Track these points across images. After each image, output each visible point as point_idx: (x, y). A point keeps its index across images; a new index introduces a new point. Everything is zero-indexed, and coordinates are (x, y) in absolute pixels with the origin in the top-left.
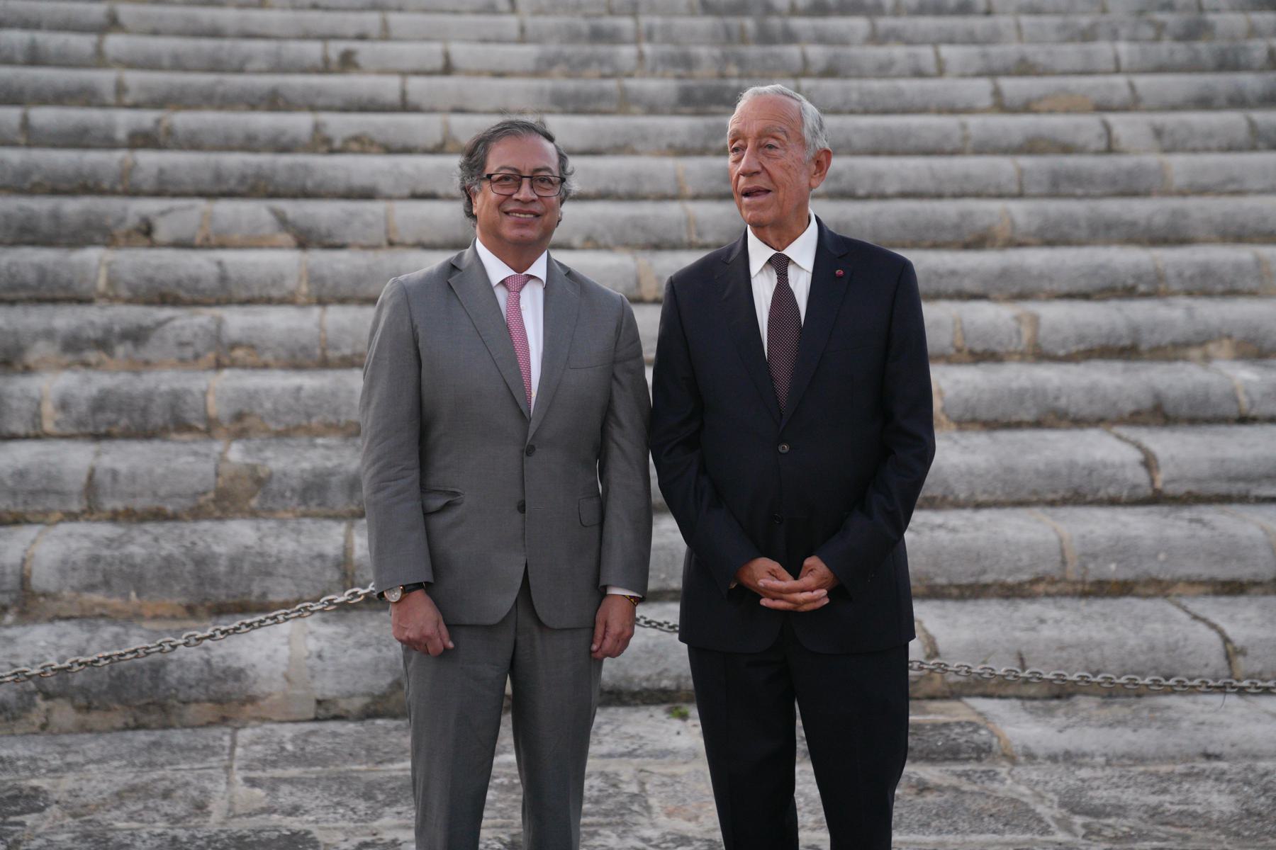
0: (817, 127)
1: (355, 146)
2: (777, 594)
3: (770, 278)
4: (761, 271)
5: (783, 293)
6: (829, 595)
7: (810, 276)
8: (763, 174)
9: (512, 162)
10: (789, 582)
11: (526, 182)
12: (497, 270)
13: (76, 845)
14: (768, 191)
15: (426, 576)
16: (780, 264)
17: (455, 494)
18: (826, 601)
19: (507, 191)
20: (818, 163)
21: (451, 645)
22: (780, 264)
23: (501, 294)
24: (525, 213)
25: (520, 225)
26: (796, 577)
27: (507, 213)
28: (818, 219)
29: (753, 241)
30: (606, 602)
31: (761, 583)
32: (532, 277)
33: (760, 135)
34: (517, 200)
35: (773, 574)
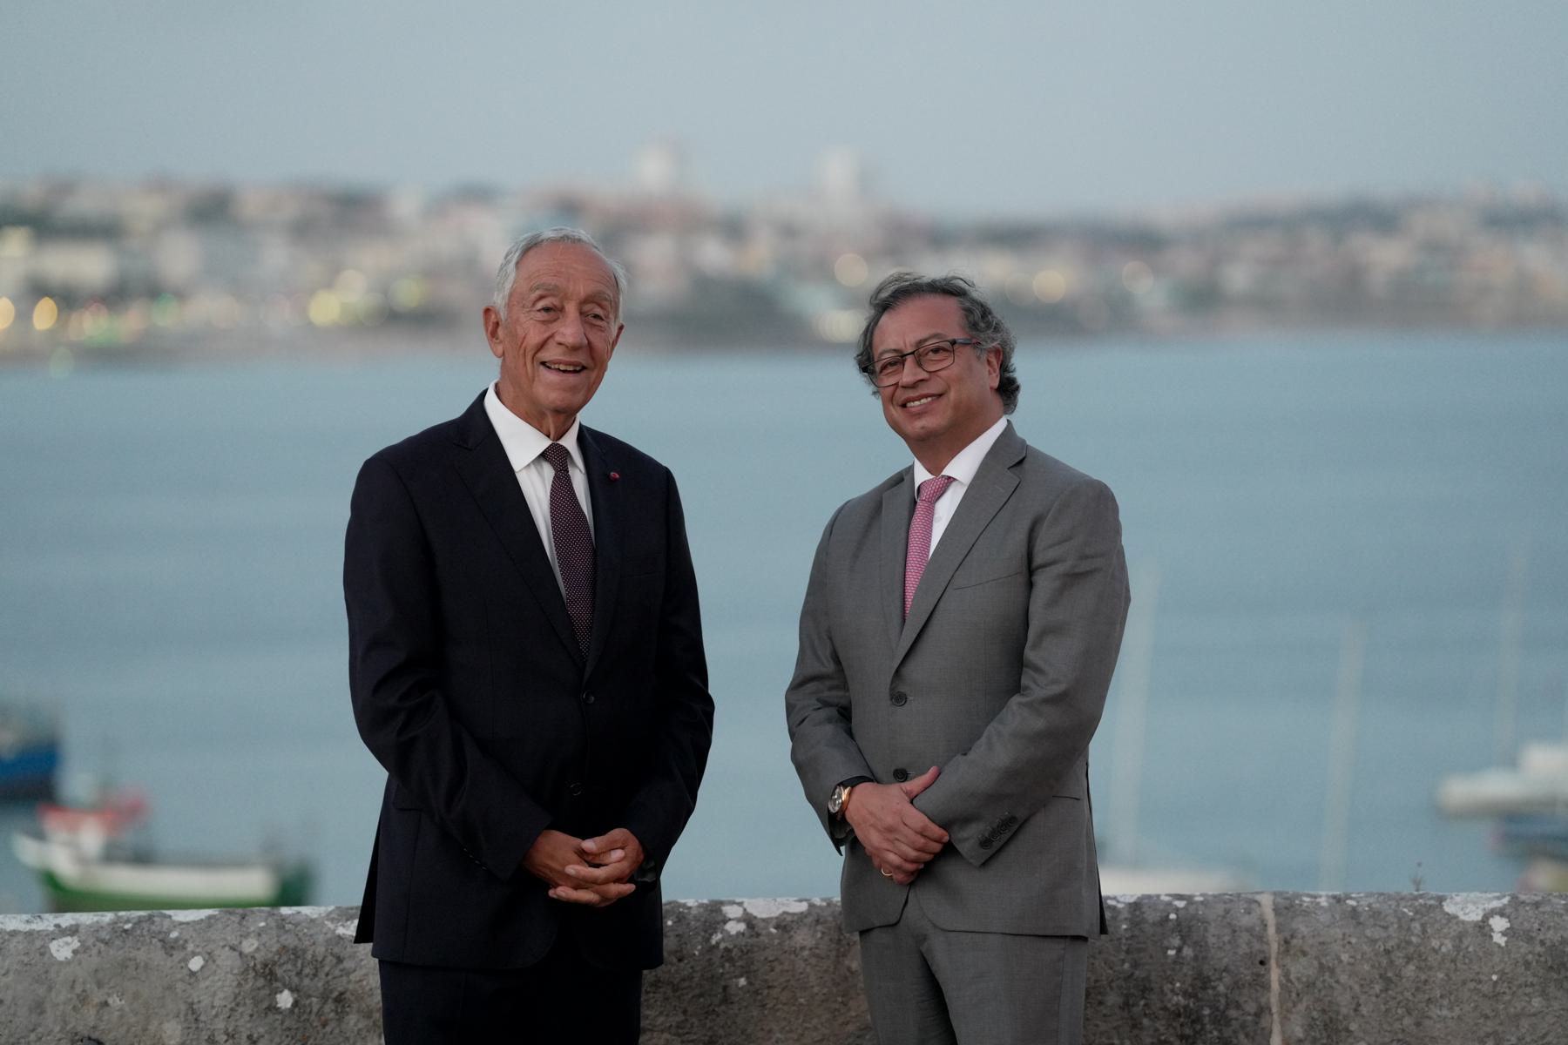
11: (910, 359)
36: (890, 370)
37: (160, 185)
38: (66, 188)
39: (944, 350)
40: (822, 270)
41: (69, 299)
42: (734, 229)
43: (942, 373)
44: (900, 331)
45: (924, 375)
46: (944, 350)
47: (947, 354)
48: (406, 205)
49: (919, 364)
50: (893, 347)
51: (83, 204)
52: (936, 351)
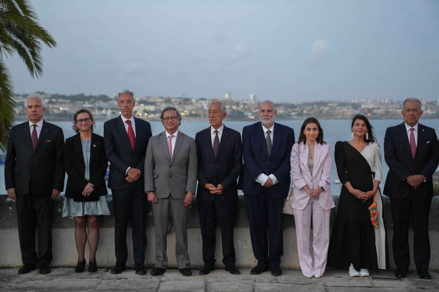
0: (224, 108)
1: (286, 117)
2: (213, 191)
3: (215, 135)
4: (213, 133)
5: (217, 137)
6: (222, 191)
7: (222, 135)
8: (214, 117)
9: (168, 116)
10: (215, 188)
11: (170, 119)
12: (168, 135)
13: (406, 291)
14: (214, 120)
15: (153, 190)
16: (216, 132)
17: (158, 175)
18: (221, 193)
19: (167, 121)
20: (224, 115)
21: (157, 202)
22: (216, 132)
23: (168, 139)
24: (171, 124)
25: (171, 126)
26: (216, 187)
27: (168, 125)
28: (224, 124)
29: (212, 128)
30: (187, 194)
31: (210, 189)
32: (174, 136)
33: (214, 111)
34: (169, 122)
35: (212, 187)
36: (167, 119)
37: (161, 98)
38: (149, 98)
39: (175, 118)
40: (249, 110)
41: (149, 112)
42: (237, 104)
43: (174, 121)
44: (166, 115)
45: (172, 121)
46: (175, 118)
47: (175, 118)
48: (193, 101)
49: (171, 119)
50: (168, 116)
51: (152, 100)
52: (173, 118)
